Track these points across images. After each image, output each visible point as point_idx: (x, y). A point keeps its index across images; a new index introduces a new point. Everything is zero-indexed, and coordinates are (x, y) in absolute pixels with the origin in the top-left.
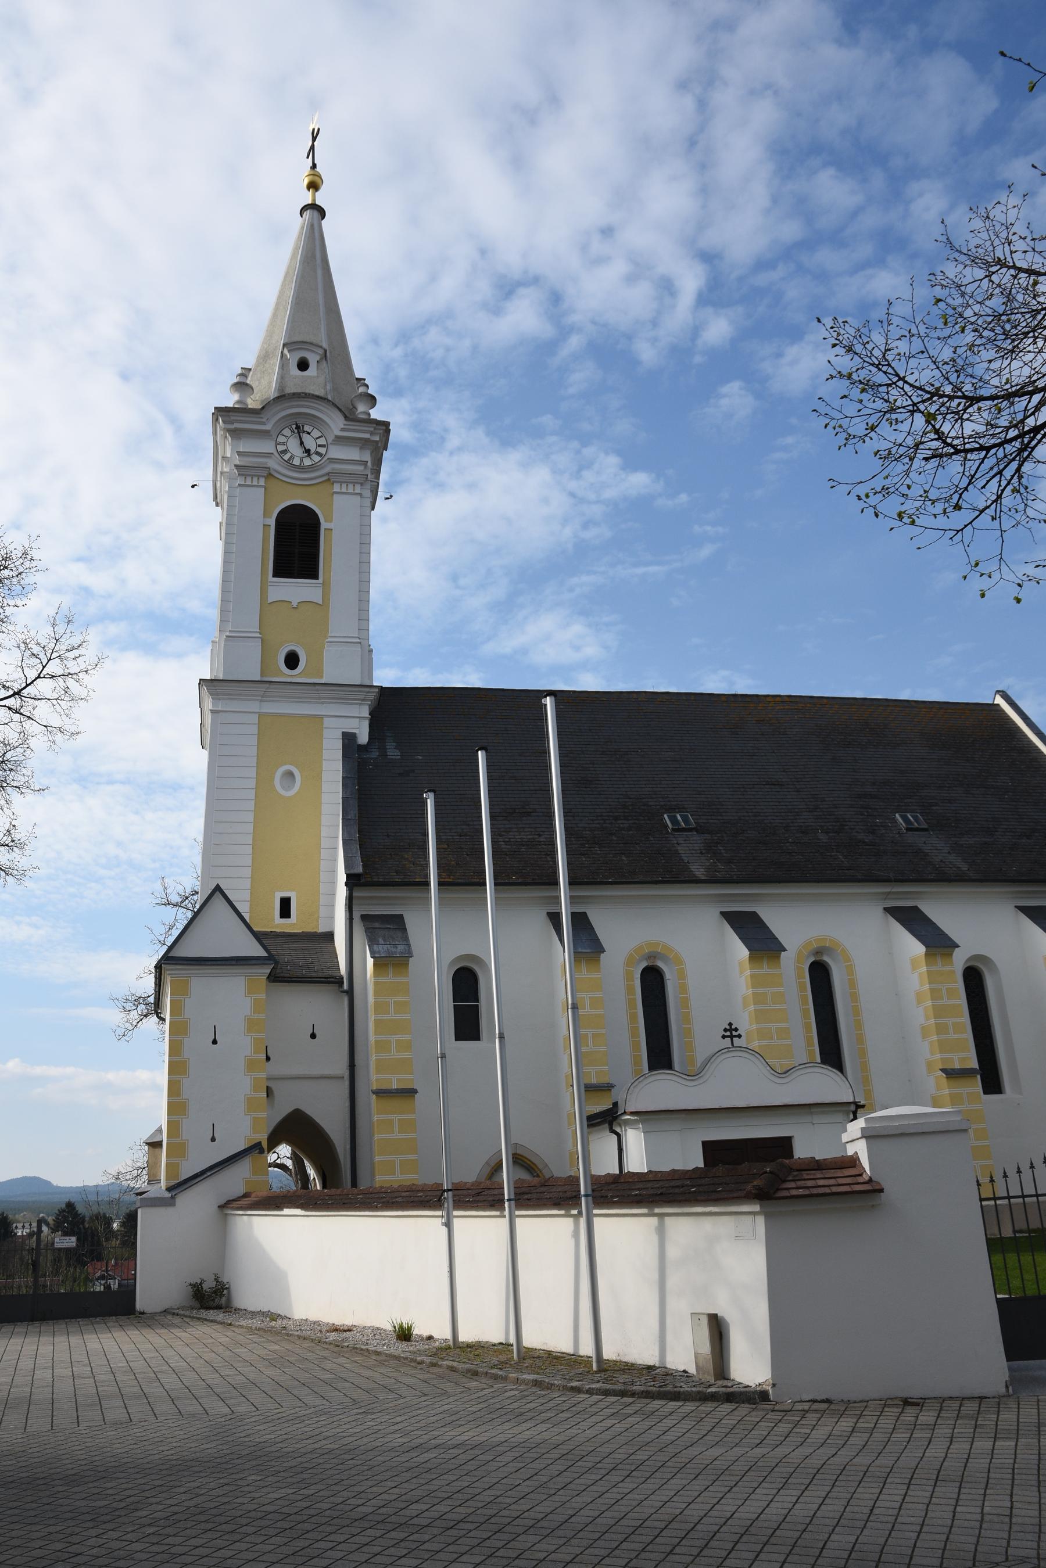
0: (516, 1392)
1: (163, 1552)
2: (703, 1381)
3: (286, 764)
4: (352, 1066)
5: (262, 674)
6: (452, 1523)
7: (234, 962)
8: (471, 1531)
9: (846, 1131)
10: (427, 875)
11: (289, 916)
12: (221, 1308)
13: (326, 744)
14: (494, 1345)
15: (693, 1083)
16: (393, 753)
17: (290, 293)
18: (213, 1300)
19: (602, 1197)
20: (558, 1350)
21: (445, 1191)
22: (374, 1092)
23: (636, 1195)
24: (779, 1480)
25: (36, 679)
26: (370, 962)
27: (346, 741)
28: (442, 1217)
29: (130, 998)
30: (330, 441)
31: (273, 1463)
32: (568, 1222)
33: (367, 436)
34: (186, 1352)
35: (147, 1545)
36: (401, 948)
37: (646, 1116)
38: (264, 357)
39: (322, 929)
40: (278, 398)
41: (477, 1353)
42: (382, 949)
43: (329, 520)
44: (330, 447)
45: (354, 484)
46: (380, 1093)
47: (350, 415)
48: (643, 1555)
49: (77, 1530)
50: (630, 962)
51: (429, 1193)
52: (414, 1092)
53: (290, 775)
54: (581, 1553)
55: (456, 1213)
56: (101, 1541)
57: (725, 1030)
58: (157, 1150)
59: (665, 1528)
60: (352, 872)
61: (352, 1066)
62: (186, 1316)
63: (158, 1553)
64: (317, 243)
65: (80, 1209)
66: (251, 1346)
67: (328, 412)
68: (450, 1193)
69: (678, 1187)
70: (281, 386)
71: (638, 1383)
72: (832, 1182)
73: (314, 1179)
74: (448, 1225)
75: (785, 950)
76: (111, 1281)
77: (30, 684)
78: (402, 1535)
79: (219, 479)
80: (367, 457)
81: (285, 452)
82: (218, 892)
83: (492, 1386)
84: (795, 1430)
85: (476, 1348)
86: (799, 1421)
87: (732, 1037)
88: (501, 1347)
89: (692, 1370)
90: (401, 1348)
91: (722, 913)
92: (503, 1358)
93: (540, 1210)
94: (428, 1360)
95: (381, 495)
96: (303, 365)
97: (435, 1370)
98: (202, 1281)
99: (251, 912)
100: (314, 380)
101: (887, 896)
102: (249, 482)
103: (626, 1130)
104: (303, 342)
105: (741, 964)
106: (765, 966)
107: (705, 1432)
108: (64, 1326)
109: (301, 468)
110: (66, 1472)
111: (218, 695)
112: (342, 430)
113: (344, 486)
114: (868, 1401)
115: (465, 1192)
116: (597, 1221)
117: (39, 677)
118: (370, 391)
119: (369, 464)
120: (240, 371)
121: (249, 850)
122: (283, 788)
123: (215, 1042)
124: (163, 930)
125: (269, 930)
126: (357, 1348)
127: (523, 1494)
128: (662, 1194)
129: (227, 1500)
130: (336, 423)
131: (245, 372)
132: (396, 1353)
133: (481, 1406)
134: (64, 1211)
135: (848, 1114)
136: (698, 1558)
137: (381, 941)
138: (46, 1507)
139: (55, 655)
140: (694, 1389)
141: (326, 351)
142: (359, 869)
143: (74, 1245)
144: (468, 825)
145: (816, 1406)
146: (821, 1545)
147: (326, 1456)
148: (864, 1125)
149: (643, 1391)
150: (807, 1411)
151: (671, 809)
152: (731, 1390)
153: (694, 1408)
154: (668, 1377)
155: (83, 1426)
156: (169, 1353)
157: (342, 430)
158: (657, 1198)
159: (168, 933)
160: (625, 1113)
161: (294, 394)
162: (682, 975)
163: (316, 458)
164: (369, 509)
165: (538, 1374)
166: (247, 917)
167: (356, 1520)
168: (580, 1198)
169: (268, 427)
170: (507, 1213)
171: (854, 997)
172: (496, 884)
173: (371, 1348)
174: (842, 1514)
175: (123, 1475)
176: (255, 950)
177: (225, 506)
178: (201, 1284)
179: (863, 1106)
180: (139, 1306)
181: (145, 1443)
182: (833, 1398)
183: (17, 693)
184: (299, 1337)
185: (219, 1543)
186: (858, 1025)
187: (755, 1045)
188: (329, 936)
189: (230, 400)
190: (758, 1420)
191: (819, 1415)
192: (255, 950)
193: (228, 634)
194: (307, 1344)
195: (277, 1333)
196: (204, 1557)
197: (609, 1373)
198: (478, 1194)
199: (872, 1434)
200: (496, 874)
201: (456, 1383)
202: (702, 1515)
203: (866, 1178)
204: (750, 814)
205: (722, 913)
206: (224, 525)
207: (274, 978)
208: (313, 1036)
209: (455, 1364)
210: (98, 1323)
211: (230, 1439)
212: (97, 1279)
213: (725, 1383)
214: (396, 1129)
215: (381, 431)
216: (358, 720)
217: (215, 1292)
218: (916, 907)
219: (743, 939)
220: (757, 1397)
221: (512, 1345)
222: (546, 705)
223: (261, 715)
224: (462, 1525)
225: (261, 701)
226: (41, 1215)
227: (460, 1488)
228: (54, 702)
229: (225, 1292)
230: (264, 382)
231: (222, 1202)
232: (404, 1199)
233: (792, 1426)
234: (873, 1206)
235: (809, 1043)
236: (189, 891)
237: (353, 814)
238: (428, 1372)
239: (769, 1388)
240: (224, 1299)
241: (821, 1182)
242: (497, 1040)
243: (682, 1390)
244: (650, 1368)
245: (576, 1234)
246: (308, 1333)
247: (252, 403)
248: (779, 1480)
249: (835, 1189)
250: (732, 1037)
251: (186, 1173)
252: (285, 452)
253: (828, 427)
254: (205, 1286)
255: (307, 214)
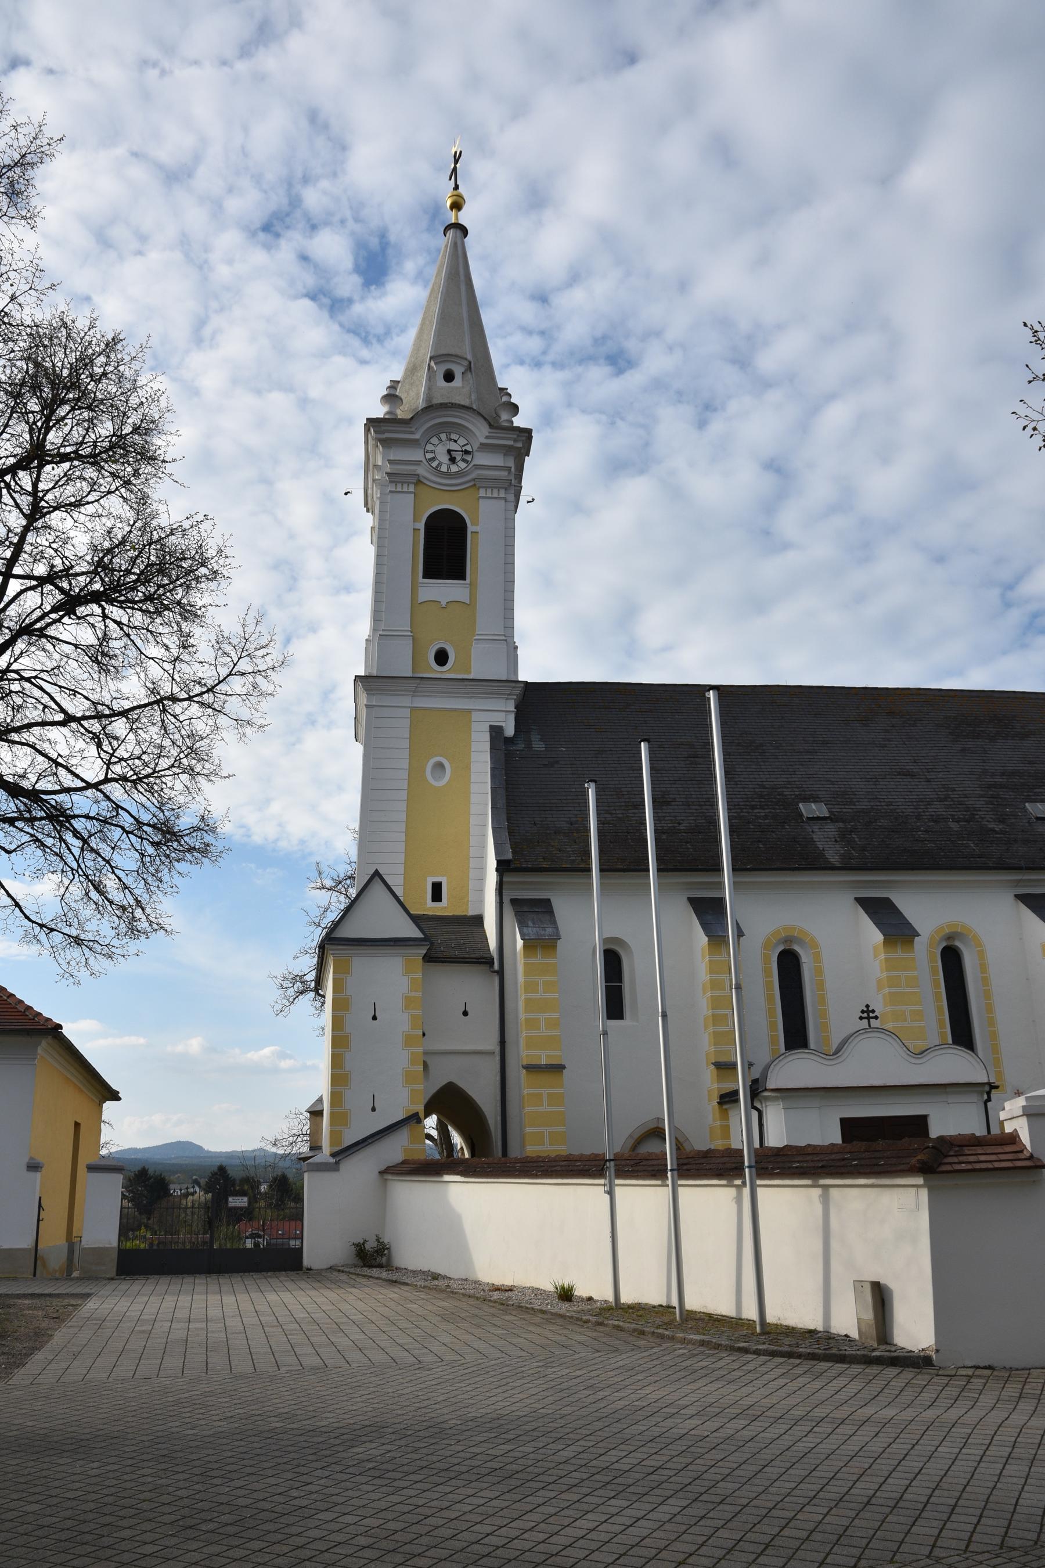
0: (685, 1351)
1: (386, 1485)
2: (866, 1345)
3: (436, 756)
4: (503, 1042)
5: (414, 670)
6: (652, 1469)
7: (392, 943)
8: (671, 1477)
9: (1004, 1109)
10: (590, 863)
11: (440, 900)
12: (382, 1267)
13: (474, 736)
14: (654, 1307)
15: (906, 1057)
16: (538, 745)
17: (436, 309)
18: (375, 1259)
19: (763, 1168)
20: (719, 1313)
21: (607, 1161)
22: (524, 1067)
23: (797, 1167)
24: (958, 1440)
25: (228, 676)
26: (520, 943)
27: (494, 734)
28: (605, 1185)
29: (287, 976)
30: (475, 448)
31: (469, 1410)
32: (732, 1192)
33: (511, 443)
34: (360, 1305)
35: (370, 1478)
36: (549, 931)
37: (788, 1094)
38: (412, 370)
39: (471, 912)
40: (426, 408)
41: (639, 1313)
42: (531, 931)
43: (475, 523)
44: (476, 454)
45: (499, 488)
46: (530, 1068)
47: (493, 424)
48: (841, 1504)
49: (303, 1462)
50: (767, 945)
51: (587, 1163)
52: (561, 1068)
53: (440, 766)
54: (781, 1501)
55: (617, 1182)
56: (327, 1473)
57: (863, 1012)
58: (318, 1118)
59: (858, 1480)
60: (503, 858)
61: (503, 1042)
62: (351, 1273)
63: (382, 1486)
64: (461, 260)
65: (231, 1173)
66: (421, 1302)
67: (471, 419)
68: (612, 1163)
69: (839, 1160)
70: (428, 397)
71: (803, 1346)
72: (993, 1157)
73: (462, 1148)
74: (611, 1193)
75: (918, 935)
76: (261, 1240)
77: (222, 681)
78: (608, 1479)
79: (370, 486)
80: (511, 463)
81: (433, 459)
82: (377, 877)
83: (660, 1345)
84: (963, 1394)
85: (637, 1309)
86: (965, 1386)
87: (869, 1018)
88: (661, 1308)
89: (854, 1334)
90: (563, 1307)
91: (856, 899)
92: (666, 1319)
93: (700, 1179)
94: (593, 1319)
95: (523, 500)
96: (449, 377)
97: (602, 1328)
98: (365, 1242)
99: (404, 896)
100: (460, 390)
101: (1018, 883)
102: (399, 489)
103: (766, 1107)
104: (449, 355)
105: (875, 948)
106: (899, 950)
107: (876, 1393)
108: (240, 1279)
109: (448, 475)
110: (279, 1410)
111: (372, 690)
112: (487, 437)
113: (405, 486)
114: (1030, 1369)
115: (623, 1163)
116: (760, 1191)
117: (230, 674)
118: (512, 400)
119: (513, 469)
120: (389, 384)
121: (403, 837)
122: (434, 778)
123: (374, 1018)
124: (318, 912)
125: (422, 913)
126: (522, 1307)
127: (714, 1445)
128: (822, 1167)
129: (433, 1441)
130: (481, 432)
131: (394, 385)
132: (562, 1312)
133: (655, 1362)
134: (216, 1174)
135: (982, 1095)
136: (895, 1510)
137: (530, 924)
138: (268, 1441)
139: (244, 654)
140: (858, 1352)
141: (470, 363)
142: (509, 856)
143: (246, 1204)
144: (611, 814)
145: (979, 1372)
146: (1014, 1502)
147: (517, 1404)
148: (1024, 1104)
149: (809, 1353)
150: (971, 1377)
151: (806, 799)
152: (895, 1354)
153: (861, 1370)
154: (831, 1341)
155: (283, 1369)
156: (345, 1307)
157: (487, 437)
158: (819, 1170)
159: (323, 915)
160: (766, 1090)
161: (441, 404)
162: (817, 957)
163: (463, 465)
164: (513, 512)
165: (704, 1334)
166: (399, 892)
167: (560, 1463)
168: (744, 1169)
169: (417, 436)
170: (669, 1182)
171: (985, 981)
172: (659, 870)
173: (536, 1307)
174: (1029, 1474)
175: (332, 1415)
176: (412, 931)
177: (377, 511)
178: (364, 1244)
179: (997, 1087)
180: (306, 1262)
181: (345, 1387)
182: (995, 1365)
183: (210, 690)
184: (464, 1295)
185: (436, 1479)
186: (990, 1008)
187: (889, 1026)
188: (479, 920)
189: (380, 411)
190: (925, 1383)
191: (984, 1381)
192: (412, 931)
193: (381, 633)
194: (472, 1302)
195: (442, 1291)
196: (425, 1491)
197: (772, 1337)
198: (637, 1164)
199: (1039, 1400)
200: (659, 859)
201: (625, 1341)
202: (891, 1469)
203: (1026, 1154)
204: (883, 804)
205: (856, 899)
206: (376, 530)
207: (428, 959)
208: (465, 1013)
209: (621, 1324)
210: (271, 1277)
211: (422, 1386)
212: (247, 1238)
213: (888, 1348)
214: (545, 1103)
215: (524, 438)
216: (504, 713)
217: (376, 1251)
218: (888, 900)
219: (877, 924)
220: (919, 1362)
221: (675, 1308)
222: (709, 698)
223: (413, 709)
224: (661, 1472)
225: (413, 696)
226: (194, 1177)
227: (652, 1438)
228: (244, 697)
229: (386, 1252)
230: (412, 394)
231: (383, 1168)
232: (563, 1168)
233: (960, 1390)
234: (1034, 1181)
235: (941, 1026)
236: (342, 876)
237: (502, 803)
238: (596, 1330)
239: (933, 1354)
240: (384, 1259)
241: (982, 1158)
242: (660, 1018)
243: (847, 1353)
244: (812, 1332)
245: (739, 1200)
246: (472, 1291)
247: (401, 413)
248: (958, 1440)
249: (997, 1165)
250: (869, 1018)
251: (349, 1139)
252: (433, 459)
253: (1027, 428)
254: (368, 1246)
255: (451, 233)
